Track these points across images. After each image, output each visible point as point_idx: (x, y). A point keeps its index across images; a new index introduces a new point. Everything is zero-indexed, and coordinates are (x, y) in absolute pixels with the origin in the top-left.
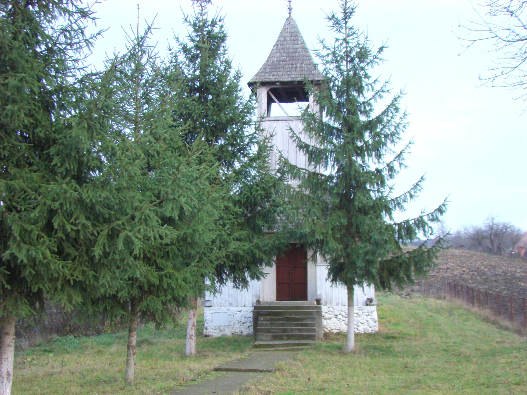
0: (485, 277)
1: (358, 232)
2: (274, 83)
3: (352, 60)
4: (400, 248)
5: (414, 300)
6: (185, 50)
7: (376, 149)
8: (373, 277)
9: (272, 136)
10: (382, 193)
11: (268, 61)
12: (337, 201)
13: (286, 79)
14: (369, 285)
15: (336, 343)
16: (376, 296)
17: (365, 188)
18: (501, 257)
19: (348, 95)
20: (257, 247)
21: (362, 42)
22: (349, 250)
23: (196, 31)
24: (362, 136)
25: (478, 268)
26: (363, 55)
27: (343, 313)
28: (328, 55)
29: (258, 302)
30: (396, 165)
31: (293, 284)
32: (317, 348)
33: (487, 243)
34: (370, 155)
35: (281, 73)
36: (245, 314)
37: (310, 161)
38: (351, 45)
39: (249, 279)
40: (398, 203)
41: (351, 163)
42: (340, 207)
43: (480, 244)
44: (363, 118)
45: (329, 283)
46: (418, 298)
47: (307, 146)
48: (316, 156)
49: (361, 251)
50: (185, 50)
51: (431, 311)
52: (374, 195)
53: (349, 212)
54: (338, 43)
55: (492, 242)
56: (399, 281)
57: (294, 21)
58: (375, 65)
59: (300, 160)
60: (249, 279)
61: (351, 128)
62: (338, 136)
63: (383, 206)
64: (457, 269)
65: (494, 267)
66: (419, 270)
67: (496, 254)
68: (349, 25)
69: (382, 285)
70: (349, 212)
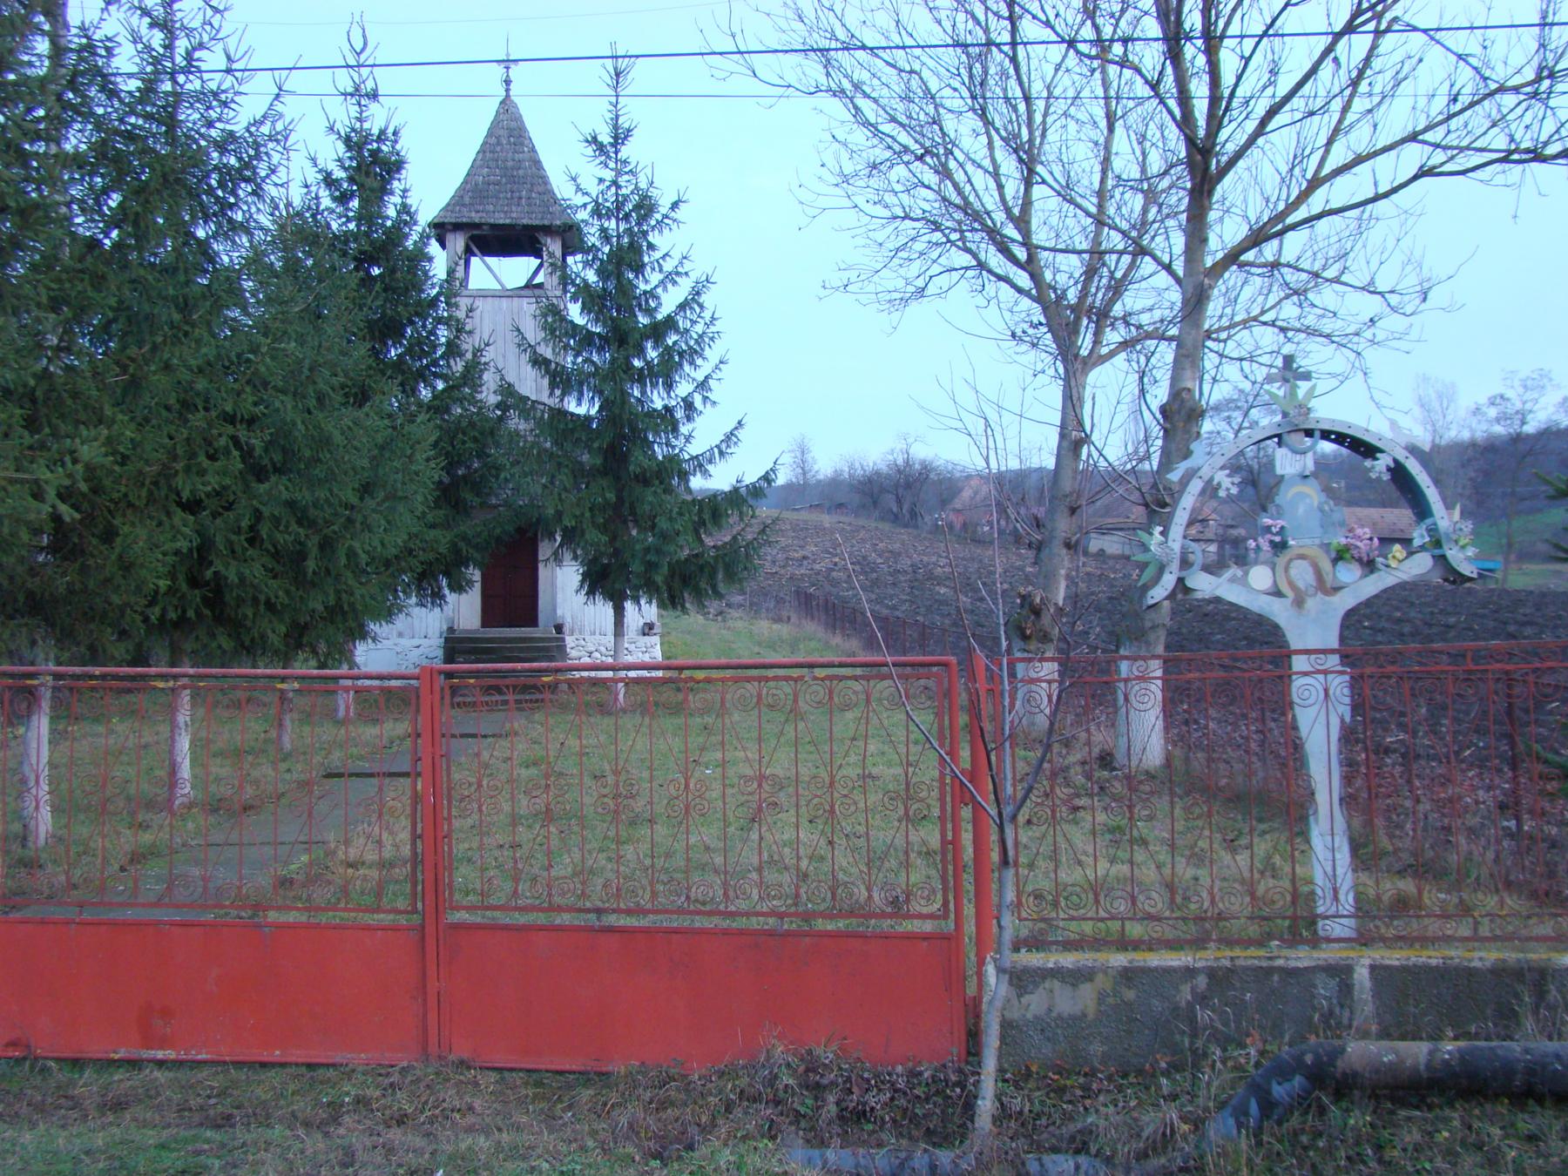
0: (874, 575)
1: (633, 512)
2: (478, 226)
3: (627, 217)
4: (701, 541)
5: (730, 623)
6: (329, 181)
7: (666, 372)
8: (658, 590)
9: (487, 345)
10: (673, 447)
11: (465, 182)
12: (598, 461)
13: (502, 220)
14: (650, 602)
15: (594, 694)
16: (660, 616)
17: (646, 438)
18: (915, 532)
19: (618, 278)
20: (464, 538)
21: (643, 185)
22: (618, 544)
23: (349, 148)
24: (641, 352)
25: (865, 558)
26: (646, 207)
27: (603, 649)
28: (585, 206)
29: (451, 629)
30: (697, 400)
31: (513, 599)
32: (564, 708)
33: (889, 501)
34: (654, 385)
35: (491, 208)
36: (426, 651)
37: (553, 386)
38: (624, 191)
39: (446, 591)
40: (700, 464)
41: (625, 395)
42: (604, 471)
43: (875, 503)
44: (643, 320)
45: (582, 597)
46: (738, 621)
47: (547, 362)
48: (561, 380)
49: (638, 547)
50: (329, 181)
51: (760, 644)
52: (659, 452)
53: (618, 479)
54: (602, 187)
55: (899, 501)
56: (699, 595)
57: (516, 106)
58: (666, 231)
59: (531, 384)
60: (446, 591)
61: (622, 338)
62: (600, 350)
63: (676, 469)
64: (823, 559)
65: (896, 555)
66: (731, 576)
67: (906, 526)
68: (622, 155)
69: (671, 601)
70: (618, 479)
